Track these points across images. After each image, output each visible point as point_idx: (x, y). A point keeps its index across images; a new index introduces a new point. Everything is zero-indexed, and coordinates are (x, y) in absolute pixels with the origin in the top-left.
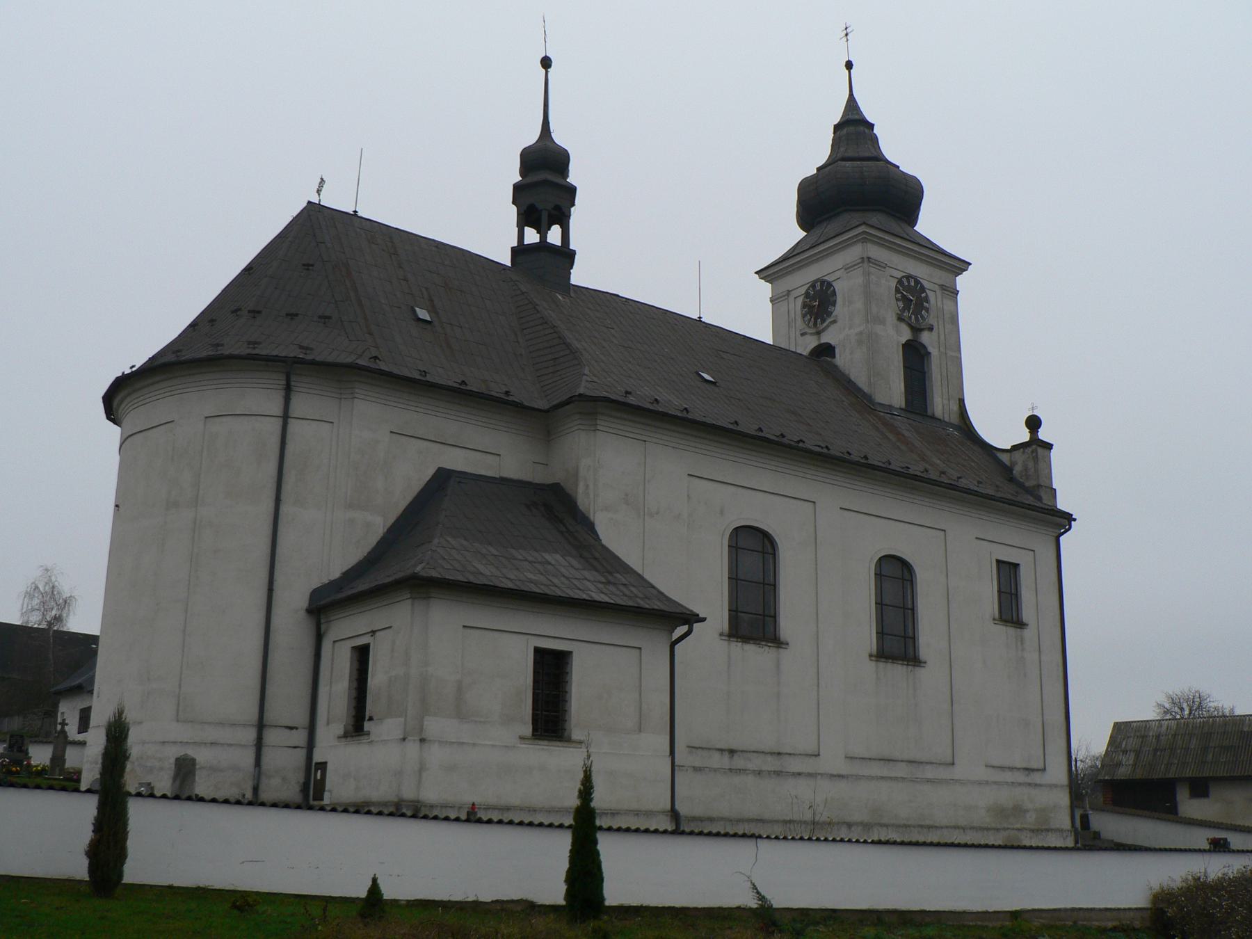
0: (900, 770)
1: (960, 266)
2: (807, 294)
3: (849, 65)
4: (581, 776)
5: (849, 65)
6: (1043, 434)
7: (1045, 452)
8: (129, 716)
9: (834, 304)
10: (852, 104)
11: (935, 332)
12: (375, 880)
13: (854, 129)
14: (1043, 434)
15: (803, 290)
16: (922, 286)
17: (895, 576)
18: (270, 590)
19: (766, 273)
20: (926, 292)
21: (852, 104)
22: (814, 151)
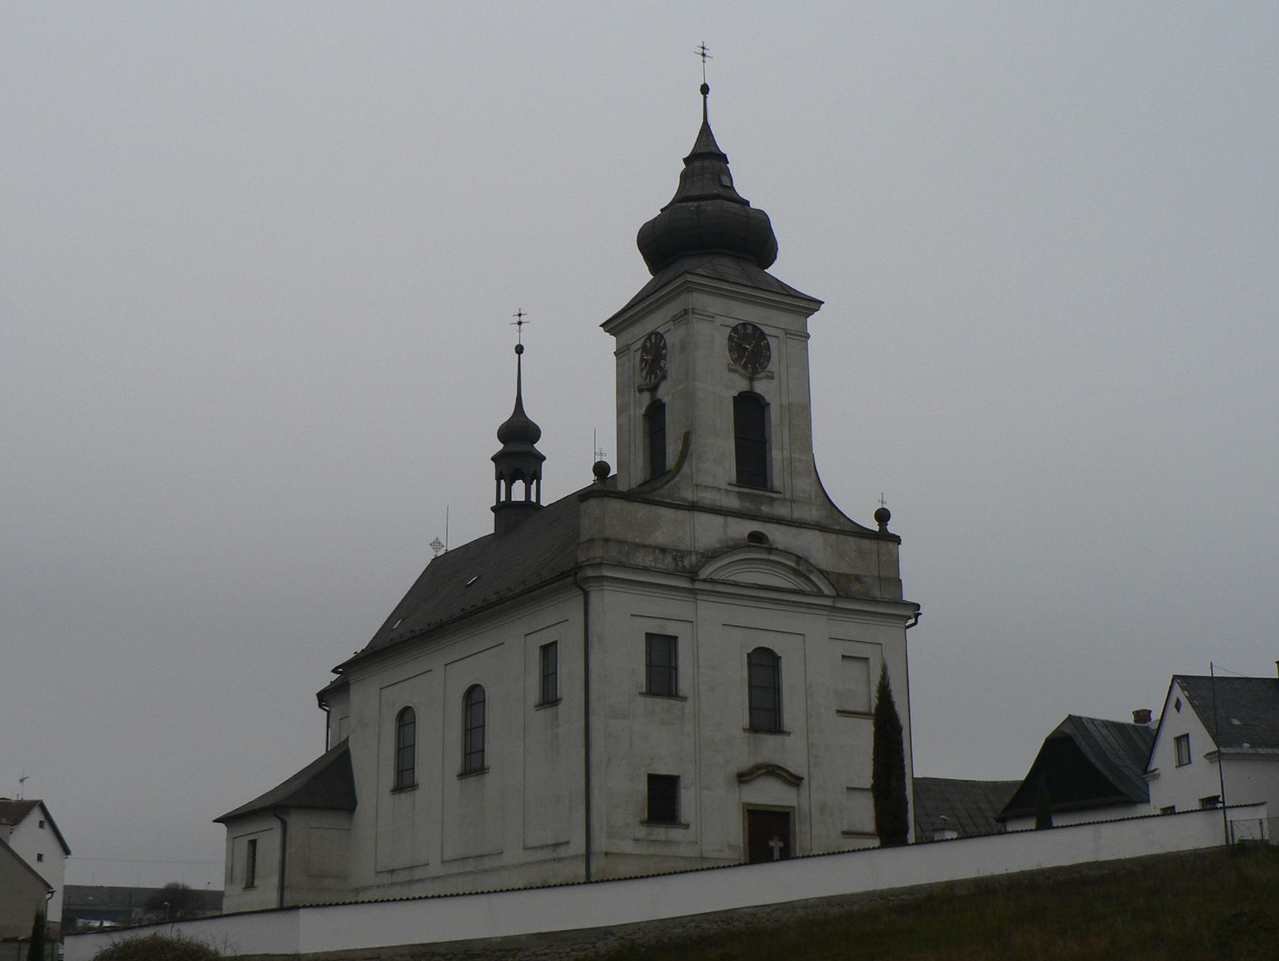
0: (469, 866)
1: (812, 305)
3: (705, 89)
5: (705, 89)
6: (892, 528)
7: (891, 545)
9: (768, 359)
10: (706, 130)
11: (775, 382)
12: (216, 821)
13: (706, 161)
14: (892, 528)
15: (639, 344)
16: (762, 332)
17: (764, 666)
20: (770, 330)
21: (706, 130)
22: (658, 189)
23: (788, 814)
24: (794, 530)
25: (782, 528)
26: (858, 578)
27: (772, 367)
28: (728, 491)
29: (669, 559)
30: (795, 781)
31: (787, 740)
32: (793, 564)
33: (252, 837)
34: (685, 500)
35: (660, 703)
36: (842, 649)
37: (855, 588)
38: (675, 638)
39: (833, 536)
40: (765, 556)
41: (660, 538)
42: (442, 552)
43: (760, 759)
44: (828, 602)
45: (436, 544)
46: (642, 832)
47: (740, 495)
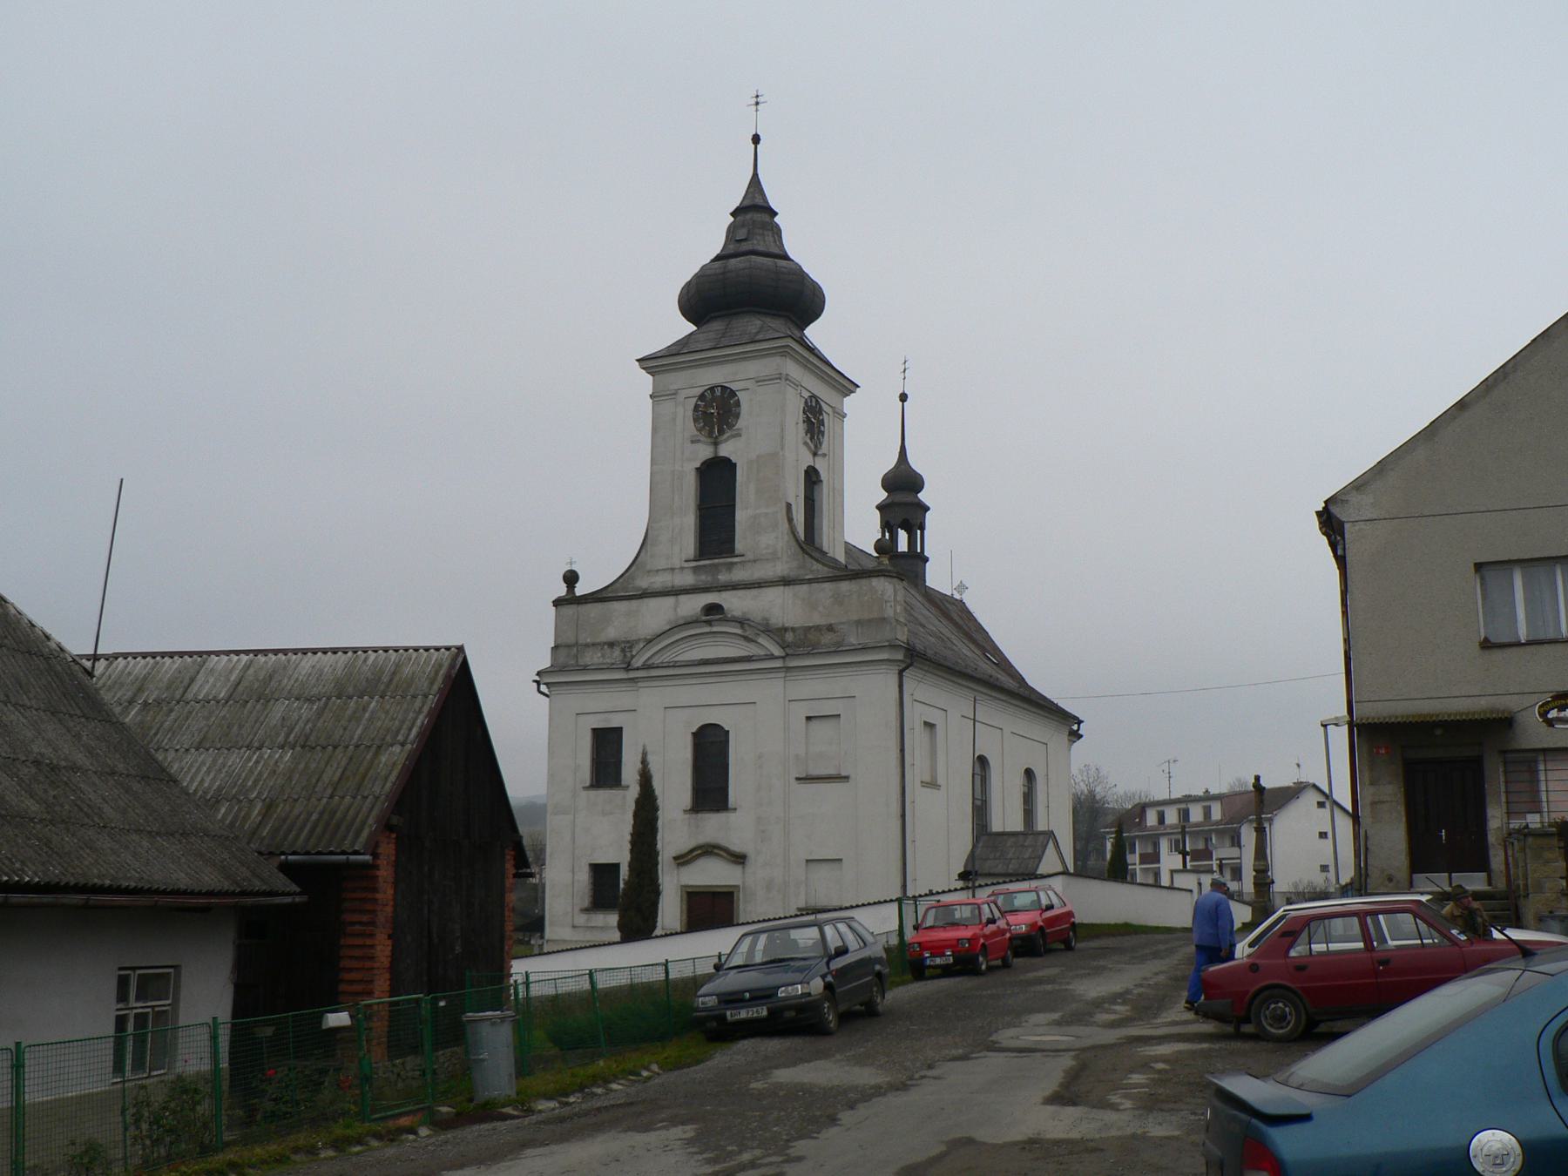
2: (702, 397)
3: (756, 139)
4: (639, 766)
5: (756, 139)
8: (649, 749)
9: (737, 416)
10: (755, 182)
13: (754, 213)
18: (902, 750)
19: (649, 363)
21: (755, 182)
22: (703, 242)
23: (689, 894)
24: (754, 592)
25: (740, 593)
26: (830, 628)
27: (741, 423)
28: (682, 568)
29: (617, 652)
30: (739, 859)
31: (732, 816)
32: (739, 631)
33: (1330, 835)
34: (639, 589)
35: (603, 794)
36: (804, 710)
37: (827, 638)
38: (621, 729)
39: (805, 587)
40: (707, 629)
41: (611, 633)
42: (957, 596)
43: (702, 840)
44: (778, 664)
45: (962, 587)
46: (582, 919)
47: (696, 570)
